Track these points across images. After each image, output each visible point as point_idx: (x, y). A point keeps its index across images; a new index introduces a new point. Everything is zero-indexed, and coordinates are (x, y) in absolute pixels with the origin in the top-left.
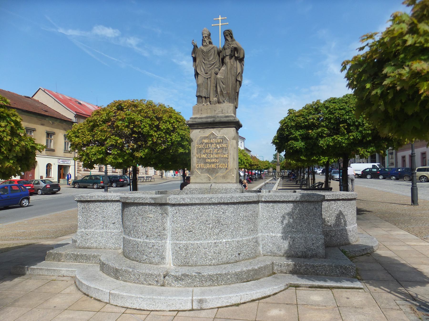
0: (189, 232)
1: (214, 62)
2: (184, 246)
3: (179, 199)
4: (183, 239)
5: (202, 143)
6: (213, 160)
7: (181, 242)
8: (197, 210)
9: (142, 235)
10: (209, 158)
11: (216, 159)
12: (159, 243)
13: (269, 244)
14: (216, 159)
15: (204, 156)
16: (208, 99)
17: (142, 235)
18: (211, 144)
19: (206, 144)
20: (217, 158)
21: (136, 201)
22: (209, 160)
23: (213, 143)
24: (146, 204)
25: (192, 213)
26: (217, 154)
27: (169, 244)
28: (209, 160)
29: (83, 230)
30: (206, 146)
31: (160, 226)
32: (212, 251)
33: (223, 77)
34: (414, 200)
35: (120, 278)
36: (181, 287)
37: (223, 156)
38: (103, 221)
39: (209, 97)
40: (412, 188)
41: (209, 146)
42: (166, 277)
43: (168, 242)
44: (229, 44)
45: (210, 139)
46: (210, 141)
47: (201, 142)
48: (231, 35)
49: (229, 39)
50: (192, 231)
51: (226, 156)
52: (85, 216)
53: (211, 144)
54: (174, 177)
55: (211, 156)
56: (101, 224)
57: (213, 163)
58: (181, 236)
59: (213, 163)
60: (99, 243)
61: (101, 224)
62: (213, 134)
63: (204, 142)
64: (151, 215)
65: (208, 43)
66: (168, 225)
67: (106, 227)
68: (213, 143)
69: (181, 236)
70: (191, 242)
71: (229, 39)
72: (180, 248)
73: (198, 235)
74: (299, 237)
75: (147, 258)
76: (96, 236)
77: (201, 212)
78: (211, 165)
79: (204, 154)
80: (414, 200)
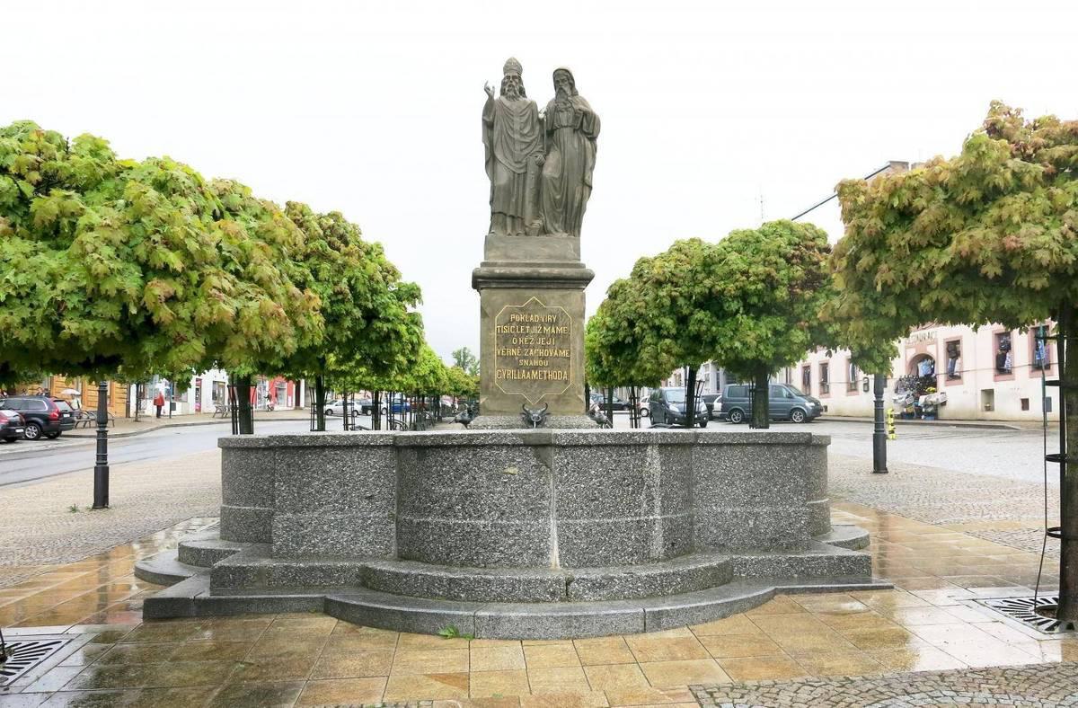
0: (593, 500)
1: (531, 138)
2: (584, 529)
3: (576, 436)
4: (582, 515)
5: (510, 322)
6: (536, 363)
7: (578, 521)
8: (607, 459)
9: (489, 512)
10: (525, 358)
11: (543, 360)
12: (532, 526)
13: (712, 529)
14: (543, 360)
15: (514, 352)
16: (518, 222)
17: (489, 512)
18: (532, 324)
19: (520, 323)
20: (544, 358)
21: (474, 442)
22: (526, 362)
23: (535, 324)
24: (500, 446)
25: (599, 464)
26: (544, 347)
27: (553, 525)
28: (526, 362)
29: (289, 515)
30: (519, 330)
31: (533, 491)
32: (633, 537)
33: (557, 176)
34: (880, 465)
35: (462, 595)
36: (600, 600)
37: (558, 352)
38: (343, 494)
39: (519, 215)
40: (874, 435)
41: (525, 330)
42: (572, 584)
43: (552, 521)
44: (567, 100)
45: (530, 315)
46: (529, 319)
47: (508, 319)
48: (571, 81)
49: (567, 89)
50: (598, 500)
51: (564, 353)
52: (294, 483)
53: (532, 324)
54: (170, 416)
55: (531, 353)
56: (336, 501)
57: (536, 368)
58: (576, 510)
59: (536, 368)
60: (333, 544)
61: (336, 501)
62: (537, 303)
63: (514, 320)
64: (511, 470)
65: (518, 93)
66: (553, 489)
67: (349, 507)
68: (535, 324)
69: (576, 510)
70: (597, 521)
71: (567, 89)
72: (575, 532)
73: (610, 507)
74: (766, 513)
75: (503, 556)
76: (325, 527)
77: (615, 461)
78: (531, 373)
79: (515, 347)
80: (880, 465)
